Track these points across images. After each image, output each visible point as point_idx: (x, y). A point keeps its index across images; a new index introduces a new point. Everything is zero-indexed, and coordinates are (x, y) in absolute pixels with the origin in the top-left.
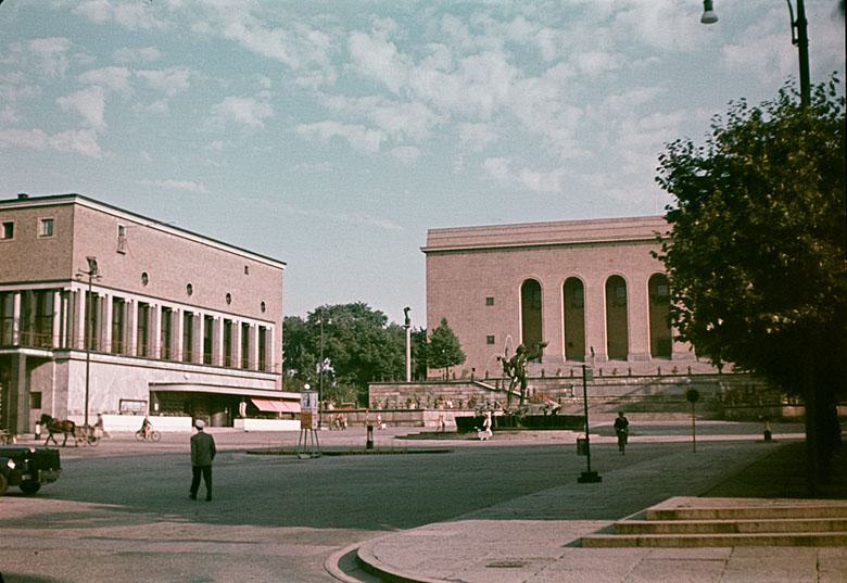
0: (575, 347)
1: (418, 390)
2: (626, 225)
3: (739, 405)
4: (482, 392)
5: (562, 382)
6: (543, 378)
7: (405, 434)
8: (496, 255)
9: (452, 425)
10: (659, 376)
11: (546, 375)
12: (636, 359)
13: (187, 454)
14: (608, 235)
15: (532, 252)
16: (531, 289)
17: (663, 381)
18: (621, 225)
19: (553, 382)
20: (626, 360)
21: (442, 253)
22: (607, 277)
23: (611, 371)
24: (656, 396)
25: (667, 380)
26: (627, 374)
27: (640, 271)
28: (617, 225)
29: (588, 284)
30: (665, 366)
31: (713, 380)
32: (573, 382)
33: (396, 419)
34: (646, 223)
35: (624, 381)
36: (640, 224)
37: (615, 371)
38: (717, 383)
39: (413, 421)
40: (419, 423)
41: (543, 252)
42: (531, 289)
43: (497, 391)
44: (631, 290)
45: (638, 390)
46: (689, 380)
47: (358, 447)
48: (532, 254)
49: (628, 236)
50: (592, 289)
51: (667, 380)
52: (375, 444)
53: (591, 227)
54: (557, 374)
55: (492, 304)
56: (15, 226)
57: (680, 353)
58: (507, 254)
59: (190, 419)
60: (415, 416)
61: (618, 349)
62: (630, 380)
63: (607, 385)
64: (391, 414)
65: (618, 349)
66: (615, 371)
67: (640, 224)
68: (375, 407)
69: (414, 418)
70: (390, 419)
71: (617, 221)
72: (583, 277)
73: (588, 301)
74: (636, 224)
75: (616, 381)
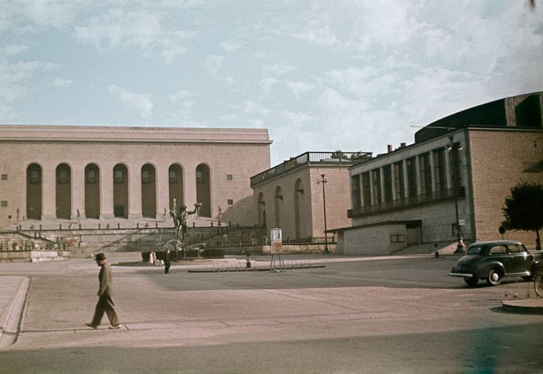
2: (101, 131)
3: (226, 245)
4: (25, 239)
5: (74, 233)
6: (60, 230)
7: (117, 263)
8: (9, 145)
9: (386, 243)
10: (138, 228)
11: (63, 228)
12: (105, 218)
13: (95, 276)
15: (261, 147)
16: (34, 171)
17: (141, 232)
18: (29, 130)
19: (68, 233)
20: (98, 218)
22: (86, 164)
23: (29, 227)
24: (136, 242)
25: (143, 231)
26: (117, 227)
28: (94, 130)
29: (74, 168)
30: (151, 223)
31: (172, 231)
32: (81, 233)
33: (10, 257)
34: (114, 131)
35: (115, 232)
36: (110, 131)
37: (108, 226)
39: (23, 258)
40: (28, 259)
41: (44, 145)
42: (34, 171)
45: (125, 237)
46: (157, 232)
47: (449, 253)
48: (36, 146)
49: (101, 138)
51: (143, 231)
52: (252, 265)
53: (77, 130)
54: (70, 227)
55: (6, 179)
56: (23, 212)
57: (133, 215)
58: (18, 146)
60: (25, 254)
62: (120, 232)
63: (104, 234)
64: (6, 253)
65: (121, 211)
66: (108, 226)
67: (110, 131)
68: (14, 248)
69: (24, 256)
70: (6, 257)
71: (94, 128)
72: (182, 163)
75: (110, 232)
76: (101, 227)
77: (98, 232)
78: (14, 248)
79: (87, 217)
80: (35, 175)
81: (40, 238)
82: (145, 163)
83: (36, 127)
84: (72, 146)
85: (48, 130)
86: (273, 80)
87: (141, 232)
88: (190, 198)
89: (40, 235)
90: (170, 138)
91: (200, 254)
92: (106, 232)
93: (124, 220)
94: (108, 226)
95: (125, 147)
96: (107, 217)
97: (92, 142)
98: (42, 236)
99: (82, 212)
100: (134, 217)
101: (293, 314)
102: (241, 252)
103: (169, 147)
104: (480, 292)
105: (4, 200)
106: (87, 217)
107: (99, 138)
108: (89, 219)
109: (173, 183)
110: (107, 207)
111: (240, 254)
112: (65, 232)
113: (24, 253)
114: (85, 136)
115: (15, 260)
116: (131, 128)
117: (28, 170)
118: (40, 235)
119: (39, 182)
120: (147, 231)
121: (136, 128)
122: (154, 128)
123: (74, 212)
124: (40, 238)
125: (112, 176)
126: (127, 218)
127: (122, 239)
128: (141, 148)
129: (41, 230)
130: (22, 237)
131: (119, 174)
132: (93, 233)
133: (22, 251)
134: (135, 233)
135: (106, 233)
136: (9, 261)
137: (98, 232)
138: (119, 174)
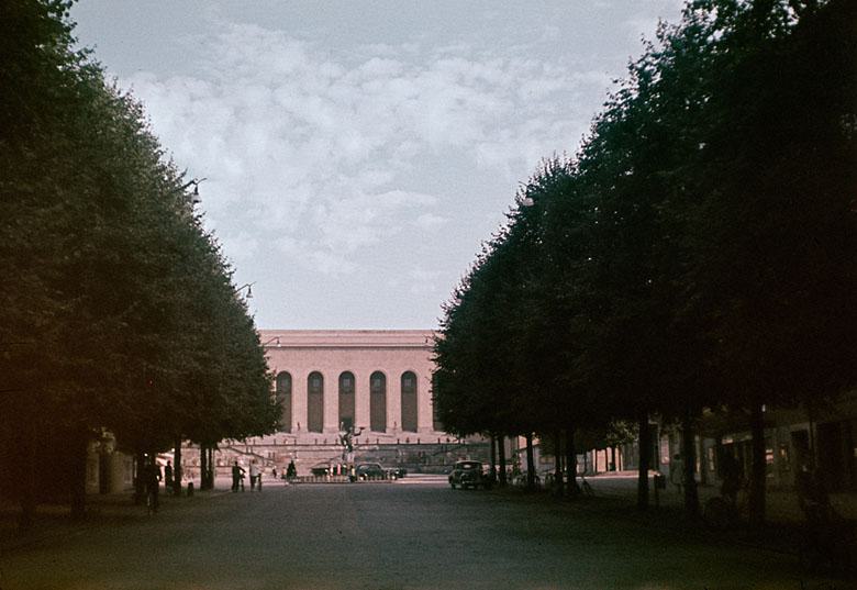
0: (347, 422)
1: (189, 453)
4: (237, 455)
5: (289, 448)
6: (275, 445)
14: (311, 342)
19: (282, 448)
21: (300, 348)
27: (426, 369)
29: (295, 376)
32: (297, 448)
35: (333, 448)
38: (397, 450)
43: (247, 454)
44: (327, 382)
50: (299, 380)
51: (361, 448)
59: (661, 504)
61: (378, 422)
65: (378, 422)
71: (319, 332)
73: (295, 389)
74: (332, 335)
75: (327, 448)
77: (315, 448)
79: (310, 430)
80: (316, 382)
81: (252, 454)
82: (310, 371)
86: (808, 428)
88: (363, 417)
90: (403, 342)
92: (323, 448)
95: (352, 353)
98: (255, 452)
99: (304, 425)
103: (403, 352)
106: (310, 430)
108: (312, 433)
109: (408, 392)
110: (331, 419)
116: (360, 332)
117: (309, 378)
119: (321, 391)
120: (366, 448)
121: (365, 332)
122: (384, 331)
123: (295, 425)
124: (252, 454)
125: (337, 384)
129: (255, 445)
131: (408, 383)
132: (309, 448)
137: (315, 448)
138: (408, 383)
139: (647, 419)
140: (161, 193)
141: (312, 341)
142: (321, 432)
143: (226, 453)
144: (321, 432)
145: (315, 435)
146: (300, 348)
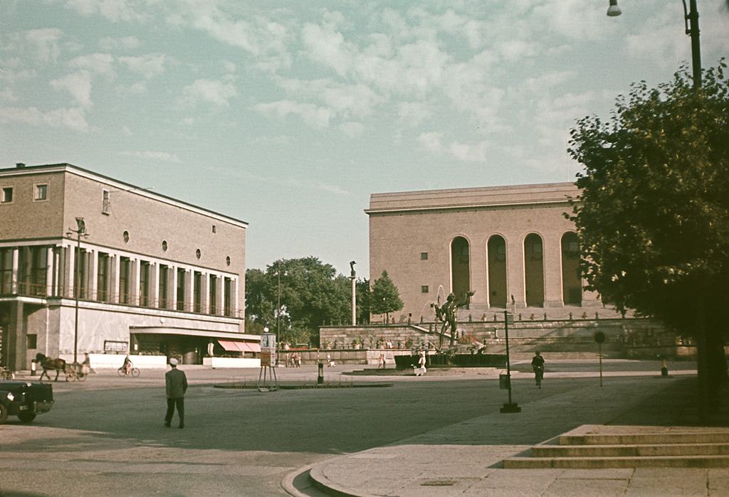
0: (498, 295)
5: (487, 326)
6: (470, 322)
16: (460, 246)
17: (574, 325)
19: (479, 326)
29: (472, 243)
30: (576, 312)
32: (496, 326)
33: (344, 358)
38: (621, 327)
41: (470, 213)
42: (460, 246)
46: (596, 324)
48: (461, 215)
50: (512, 246)
53: (512, 191)
61: (535, 296)
62: (546, 324)
63: (526, 328)
68: (325, 347)
69: (359, 357)
70: (338, 358)
74: (550, 189)
75: (534, 325)
76: (523, 319)
78: (354, 347)
83: (461, 191)
84: (505, 213)
85: (474, 194)
87: (574, 325)
89: (436, 330)
91: (451, 361)
93: (577, 308)
94: (531, 318)
96: (556, 305)
97: (531, 206)
100: (590, 303)
101: (98, 459)
102: (655, 355)
104: (622, 428)
105: (424, 285)
107: (539, 200)
111: (654, 358)
112: (475, 326)
113: (358, 353)
114: (540, 197)
115: (349, 362)
118: (436, 330)
123: (509, 298)
126: (581, 306)
127: (548, 334)
128: (435, 219)
130: (414, 331)
133: (326, 351)
134: (565, 327)
135: (528, 326)
136: (341, 362)
139: (683, 270)
140: (723, 119)
141: (529, 197)
142: (542, 306)
143: (18, 335)
144: (542, 306)
145: (533, 310)
146: (531, 206)
